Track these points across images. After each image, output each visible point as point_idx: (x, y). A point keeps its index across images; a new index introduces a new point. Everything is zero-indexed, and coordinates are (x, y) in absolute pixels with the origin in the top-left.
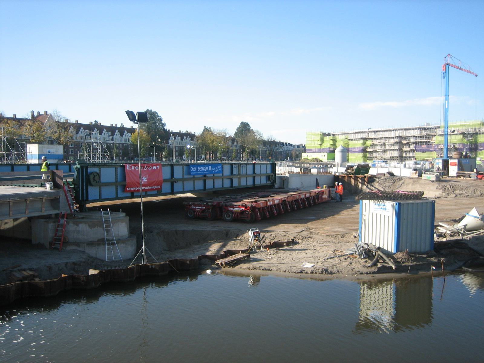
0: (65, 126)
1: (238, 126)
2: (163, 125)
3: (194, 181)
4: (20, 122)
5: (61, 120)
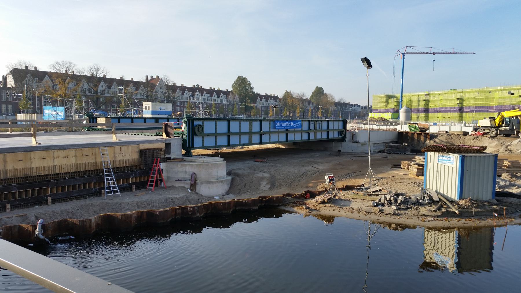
0: (173, 88)
1: (314, 90)
2: (252, 88)
3: (216, 137)
4: (137, 84)
5: (170, 83)
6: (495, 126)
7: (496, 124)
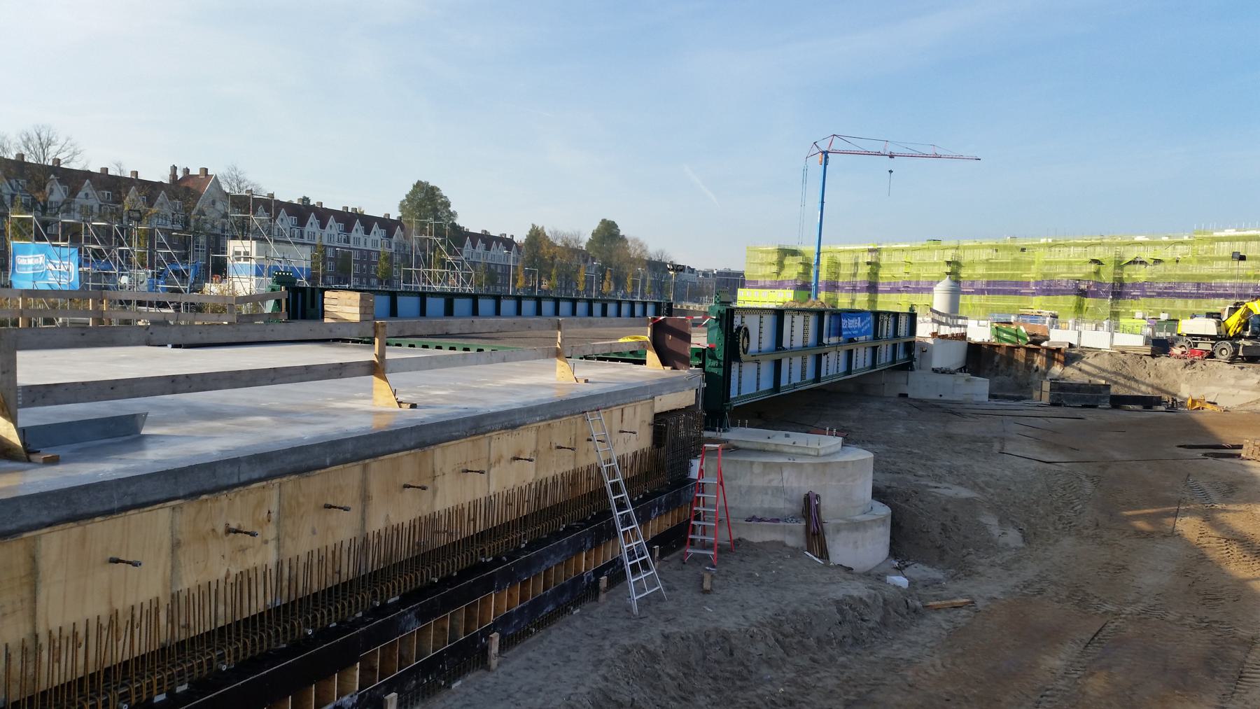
6: (1226, 336)
7: (1230, 331)
